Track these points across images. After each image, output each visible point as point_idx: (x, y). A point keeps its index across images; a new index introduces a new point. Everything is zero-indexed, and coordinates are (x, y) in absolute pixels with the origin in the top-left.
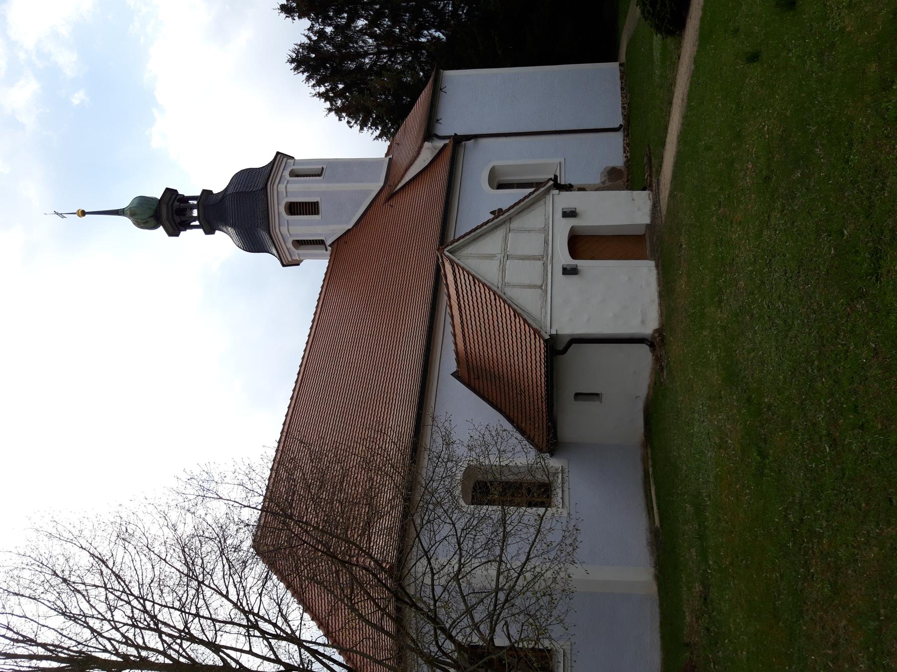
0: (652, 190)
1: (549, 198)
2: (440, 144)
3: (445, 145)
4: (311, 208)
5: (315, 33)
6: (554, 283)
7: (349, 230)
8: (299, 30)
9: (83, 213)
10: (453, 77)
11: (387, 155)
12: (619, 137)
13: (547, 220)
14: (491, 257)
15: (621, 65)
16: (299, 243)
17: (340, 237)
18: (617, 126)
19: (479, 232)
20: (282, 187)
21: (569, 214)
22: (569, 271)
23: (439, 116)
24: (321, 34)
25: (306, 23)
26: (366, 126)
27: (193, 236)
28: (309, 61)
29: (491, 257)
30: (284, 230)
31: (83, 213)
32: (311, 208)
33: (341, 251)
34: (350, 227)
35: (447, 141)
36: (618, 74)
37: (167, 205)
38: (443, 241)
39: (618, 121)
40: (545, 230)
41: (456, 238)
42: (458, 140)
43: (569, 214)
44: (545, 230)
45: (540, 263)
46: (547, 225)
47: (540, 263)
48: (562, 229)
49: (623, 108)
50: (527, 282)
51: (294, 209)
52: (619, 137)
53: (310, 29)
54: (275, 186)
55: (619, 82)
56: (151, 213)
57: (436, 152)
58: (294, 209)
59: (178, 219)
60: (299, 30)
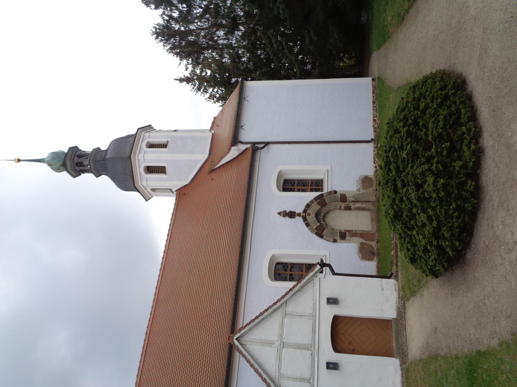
0: (397, 281)
1: (316, 280)
2: (243, 147)
3: (246, 149)
4: (161, 170)
5: (167, 16)
6: (320, 378)
7: (186, 185)
8: (155, 16)
9: (19, 160)
10: (251, 85)
11: (212, 128)
12: (371, 146)
13: (314, 304)
14: (270, 343)
15: (373, 80)
16: (153, 190)
17: (181, 188)
18: (370, 139)
19: (260, 318)
20: (141, 156)
21: (332, 301)
22: (332, 366)
23: (242, 124)
24: (171, 17)
25: (160, 11)
26: (200, 91)
27: (87, 178)
28: (164, 33)
29: (270, 343)
30: (144, 183)
31: (19, 160)
32: (161, 170)
33: (182, 194)
34: (187, 183)
35: (248, 146)
36: (371, 89)
37: (70, 160)
38: (233, 329)
39: (371, 135)
40: (313, 316)
41: (244, 325)
42: (255, 148)
43: (332, 301)
44: (313, 316)
45: (309, 353)
46: (314, 310)
47: (309, 353)
48: (328, 313)
49: (374, 120)
50: (298, 375)
51: (150, 170)
52: (371, 146)
53: (164, 13)
54: (136, 156)
55: (371, 95)
56: (61, 163)
57: (240, 152)
58: (150, 170)
59: (78, 169)
60: (155, 16)
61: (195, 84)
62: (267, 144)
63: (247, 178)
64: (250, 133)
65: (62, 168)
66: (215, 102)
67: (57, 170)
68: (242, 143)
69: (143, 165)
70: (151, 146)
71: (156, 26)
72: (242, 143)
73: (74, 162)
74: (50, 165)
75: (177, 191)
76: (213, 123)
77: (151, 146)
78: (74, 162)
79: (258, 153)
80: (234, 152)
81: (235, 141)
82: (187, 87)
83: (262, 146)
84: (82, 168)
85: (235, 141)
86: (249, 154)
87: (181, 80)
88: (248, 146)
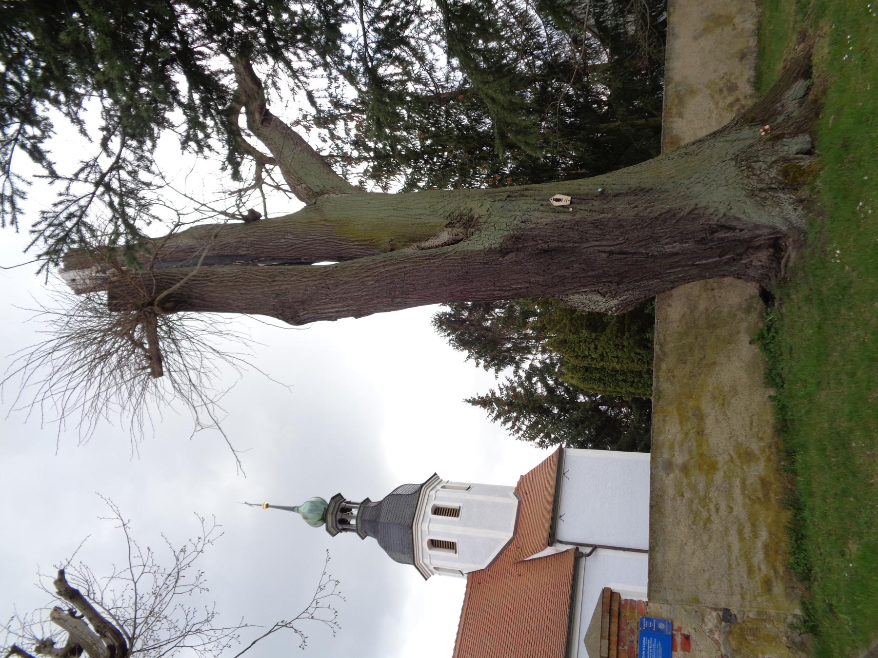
2: (562, 548)
3: (567, 551)
4: (450, 546)
9: (267, 506)
16: (435, 568)
20: (425, 526)
27: (348, 538)
30: (427, 561)
31: (267, 506)
32: (450, 546)
33: (475, 580)
35: (570, 547)
42: (578, 555)
51: (434, 544)
56: (320, 517)
58: (434, 544)
61: (494, 409)
62: (595, 547)
63: (554, 487)
64: (572, 530)
65: (321, 522)
66: (520, 438)
67: (315, 525)
68: (561, 542)
69: (427, 539)
70: (437, 511)
71: (491, 418)
72: (561, 542)
73: (336, 515)
74: (305, 518)
75: (469, 573)
76: (519, 483)
77: (437, 511)
78: (336, 515)
79: (583, 561)
80: (549, 551)
81: (552, 539)
82: (481, 412)
83: (587, 550)
84: (345, 527)
85: (552, 539)
86: (571, 559)
87: (474, 402)
88: (570, 547)
